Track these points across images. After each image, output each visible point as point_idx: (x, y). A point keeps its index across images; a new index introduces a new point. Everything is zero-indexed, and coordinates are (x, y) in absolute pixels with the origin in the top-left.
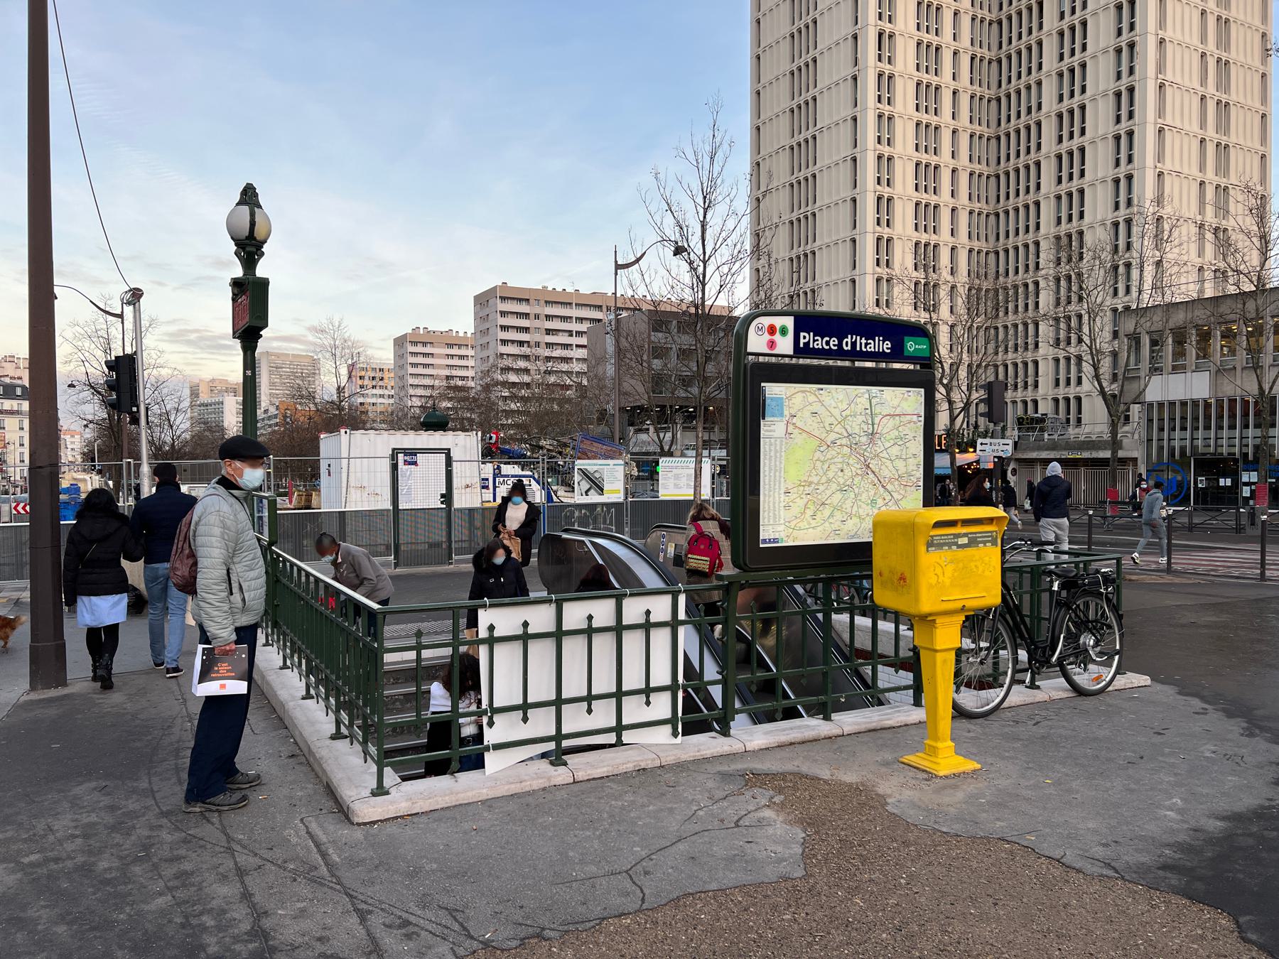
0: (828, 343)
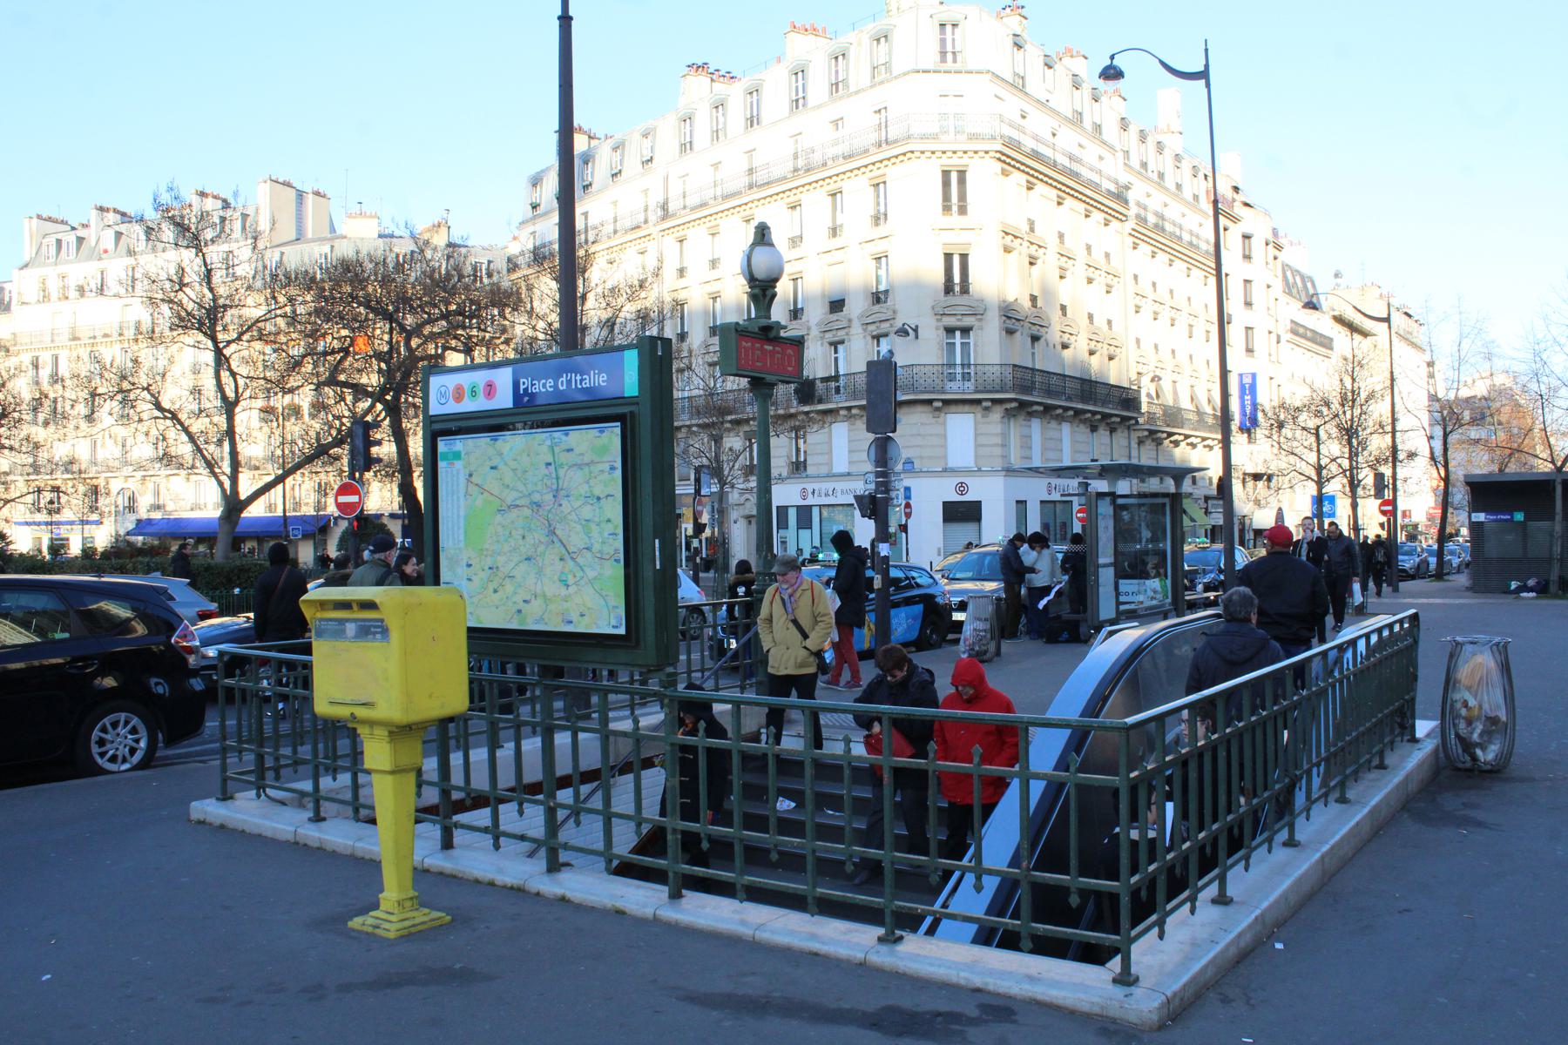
0: (544, 386)
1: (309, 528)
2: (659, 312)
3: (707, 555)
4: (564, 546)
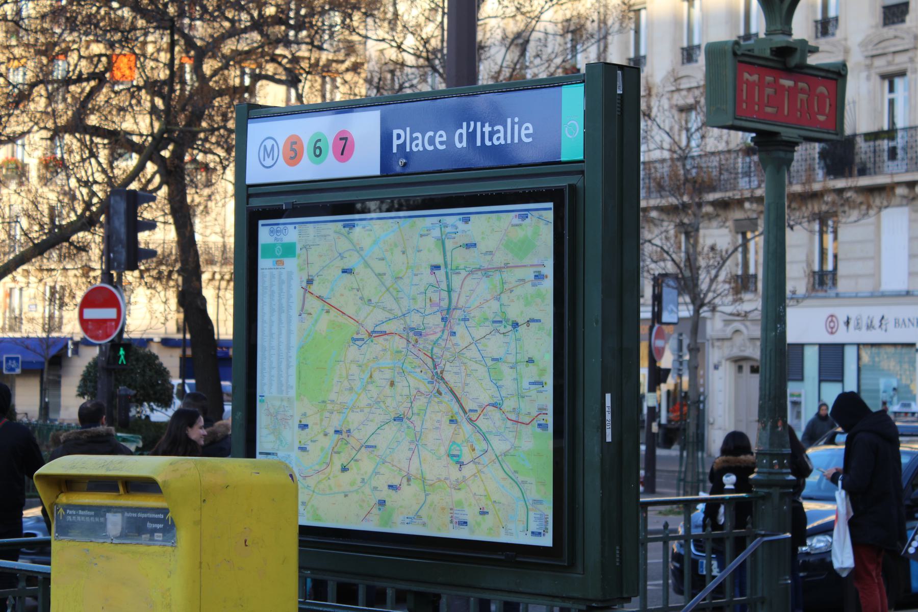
0: (432, 141)
1: (32, 358)
2: (600, 22)
3: (669, 421)
4: (458, 400)
